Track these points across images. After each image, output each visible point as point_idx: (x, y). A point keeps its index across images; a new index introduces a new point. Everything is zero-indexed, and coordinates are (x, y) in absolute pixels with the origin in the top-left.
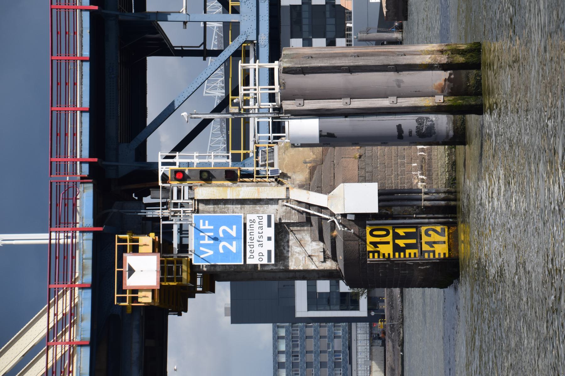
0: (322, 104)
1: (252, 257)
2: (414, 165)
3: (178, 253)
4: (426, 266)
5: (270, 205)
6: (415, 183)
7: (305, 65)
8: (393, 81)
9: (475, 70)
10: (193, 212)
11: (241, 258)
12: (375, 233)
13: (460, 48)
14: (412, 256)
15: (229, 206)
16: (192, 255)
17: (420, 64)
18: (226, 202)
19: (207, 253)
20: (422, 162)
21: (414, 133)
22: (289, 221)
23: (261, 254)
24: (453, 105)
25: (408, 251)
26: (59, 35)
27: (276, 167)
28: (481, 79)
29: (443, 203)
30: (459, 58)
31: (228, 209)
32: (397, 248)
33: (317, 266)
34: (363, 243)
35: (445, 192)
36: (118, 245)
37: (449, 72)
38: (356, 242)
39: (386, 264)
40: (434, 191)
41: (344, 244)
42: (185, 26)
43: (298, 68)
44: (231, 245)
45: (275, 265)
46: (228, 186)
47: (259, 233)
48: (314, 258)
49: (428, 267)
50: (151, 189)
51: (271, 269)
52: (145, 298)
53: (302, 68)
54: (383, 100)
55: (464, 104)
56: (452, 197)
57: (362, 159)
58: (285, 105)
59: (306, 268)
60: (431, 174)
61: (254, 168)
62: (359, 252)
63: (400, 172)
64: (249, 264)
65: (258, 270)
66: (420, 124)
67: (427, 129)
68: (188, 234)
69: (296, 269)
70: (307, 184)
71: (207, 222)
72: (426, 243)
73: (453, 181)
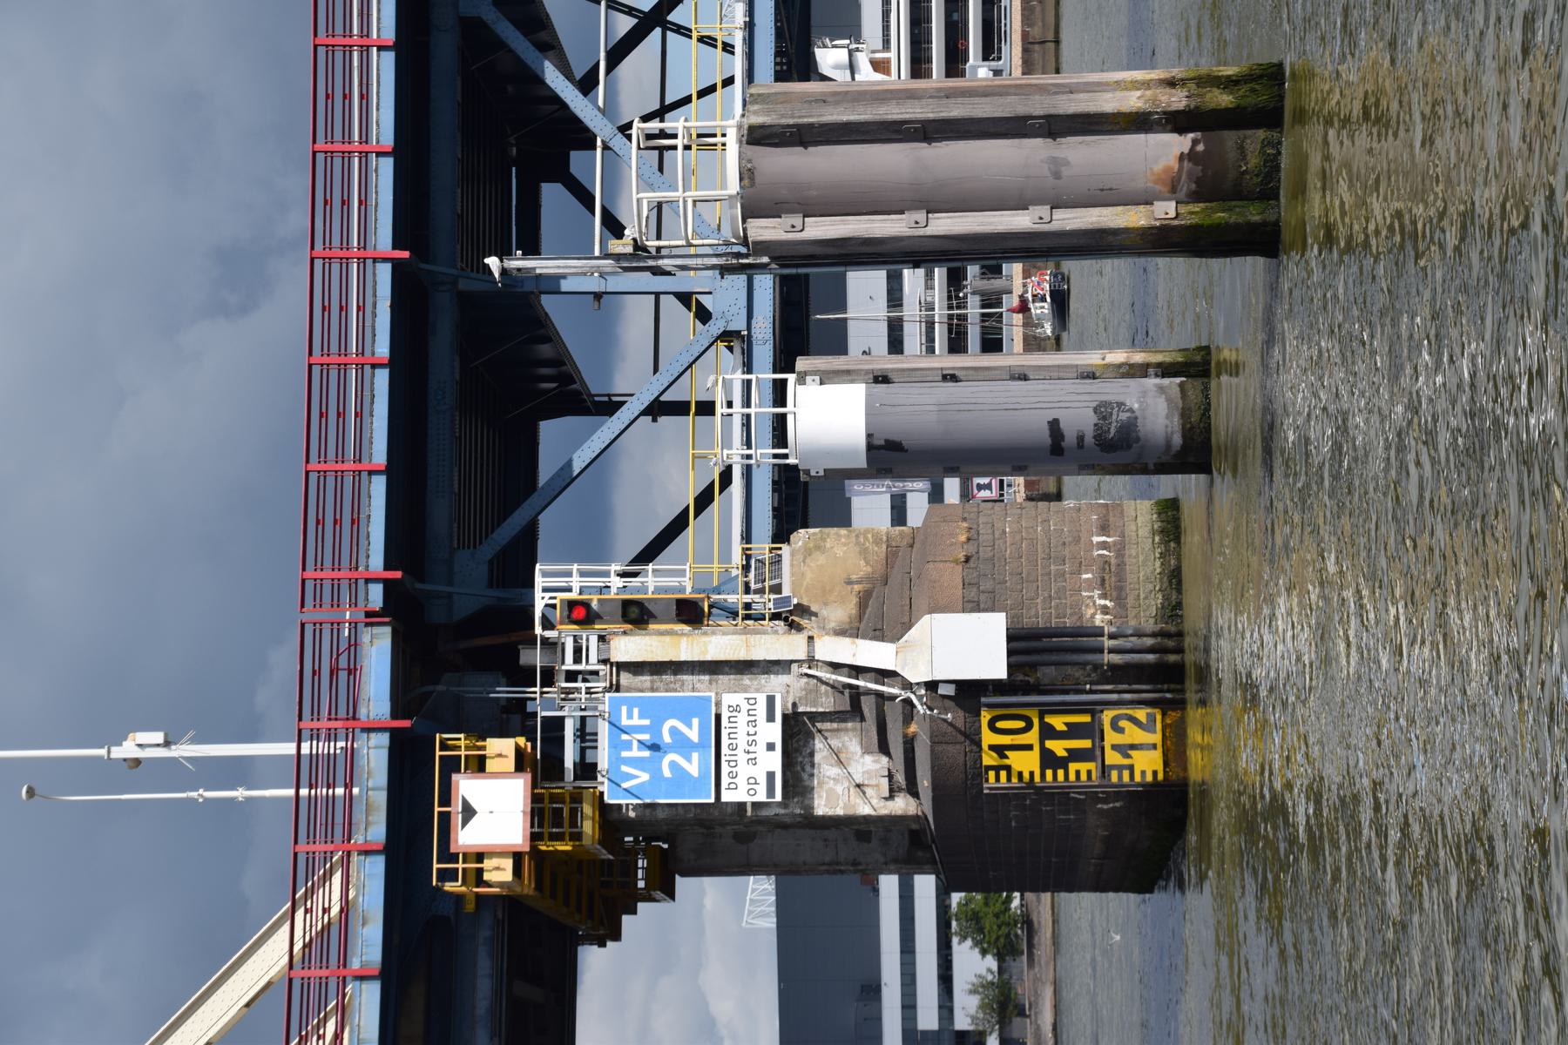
0: (850, 226)
1: (733, 786)
2: (1085, 576)
3: (576, 778)
4: (1114, 802)
5: (772, 676)
6: (1088, 616)
7: (806, 120)
8: (1042, 161)
9: (1261, 131)
10: (609, 689)
11: (710, 790)
12: (1000, 725)
13: (1220, 74)
14: (1084, 777)
15: (685, 677)
16: (603, 783)
17: (1113, 114)
18: (677, 667)
19: (636, 777)
20: (1104, 569)
21: (1089, 439)
22: (814, 710)
23: (752, 781)
24: (1202, 226)
25: (1073, 767)
26: (326, 314)
27: (786, 592)
28: (1279, 153)
29: (1151, 657)
30: (1220, 97)
31: (683, 685)
32: (1048, 759)
33: (875, 806)
34: (975, 748)
35: (1154, 635)
36: (441, 757)
37: (1191, 135)
38: (958, 746)
39: (1024, 796)
40: (1130, 632)
41: (932, 751)
42: (596, 303)
43: (789, 126)
44: (689, 760)
45: (783, 804)
46: (683, 634)
47: (748, 735)
48: (869, 791)
49: (1117, 805)
50: (520, 647)
51: (776, 815)
52: (500, 873)
53: (800, 128)
54: (1014, 215)
55: (1232, 220)
56: (1171, 643)
57: (972, 564)
58: (754, 230)
59: (850, 812)
60: (1124, 596)
61: (739, 596)
62: (966, 772)
63: (1055, 592)
64: (727, 803)
65: (484, 258)
66: (1104, 418)
67: (1119, 430)
68: (596, 741)
69: (830, 813)
70: (851, 628)
71: (636, 711)
72: (1114, 747)
73: (1173, 609)
